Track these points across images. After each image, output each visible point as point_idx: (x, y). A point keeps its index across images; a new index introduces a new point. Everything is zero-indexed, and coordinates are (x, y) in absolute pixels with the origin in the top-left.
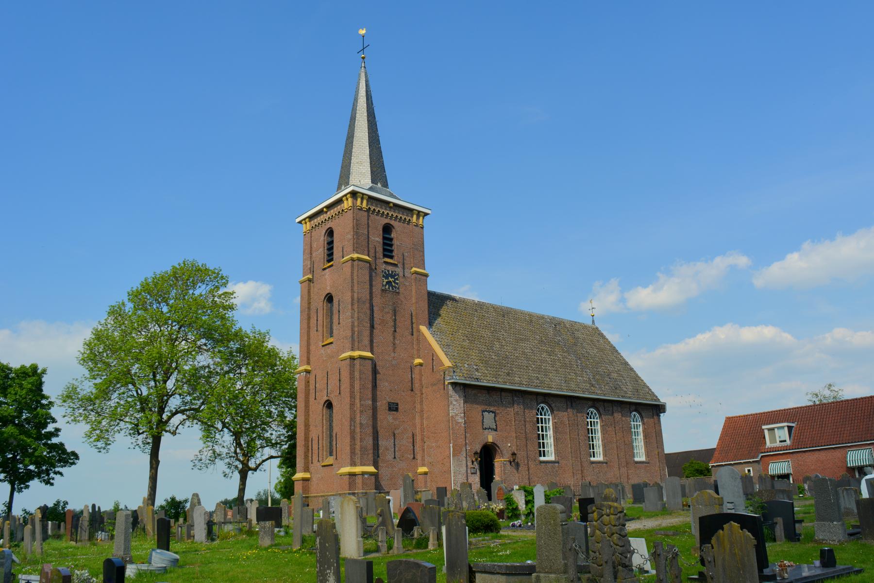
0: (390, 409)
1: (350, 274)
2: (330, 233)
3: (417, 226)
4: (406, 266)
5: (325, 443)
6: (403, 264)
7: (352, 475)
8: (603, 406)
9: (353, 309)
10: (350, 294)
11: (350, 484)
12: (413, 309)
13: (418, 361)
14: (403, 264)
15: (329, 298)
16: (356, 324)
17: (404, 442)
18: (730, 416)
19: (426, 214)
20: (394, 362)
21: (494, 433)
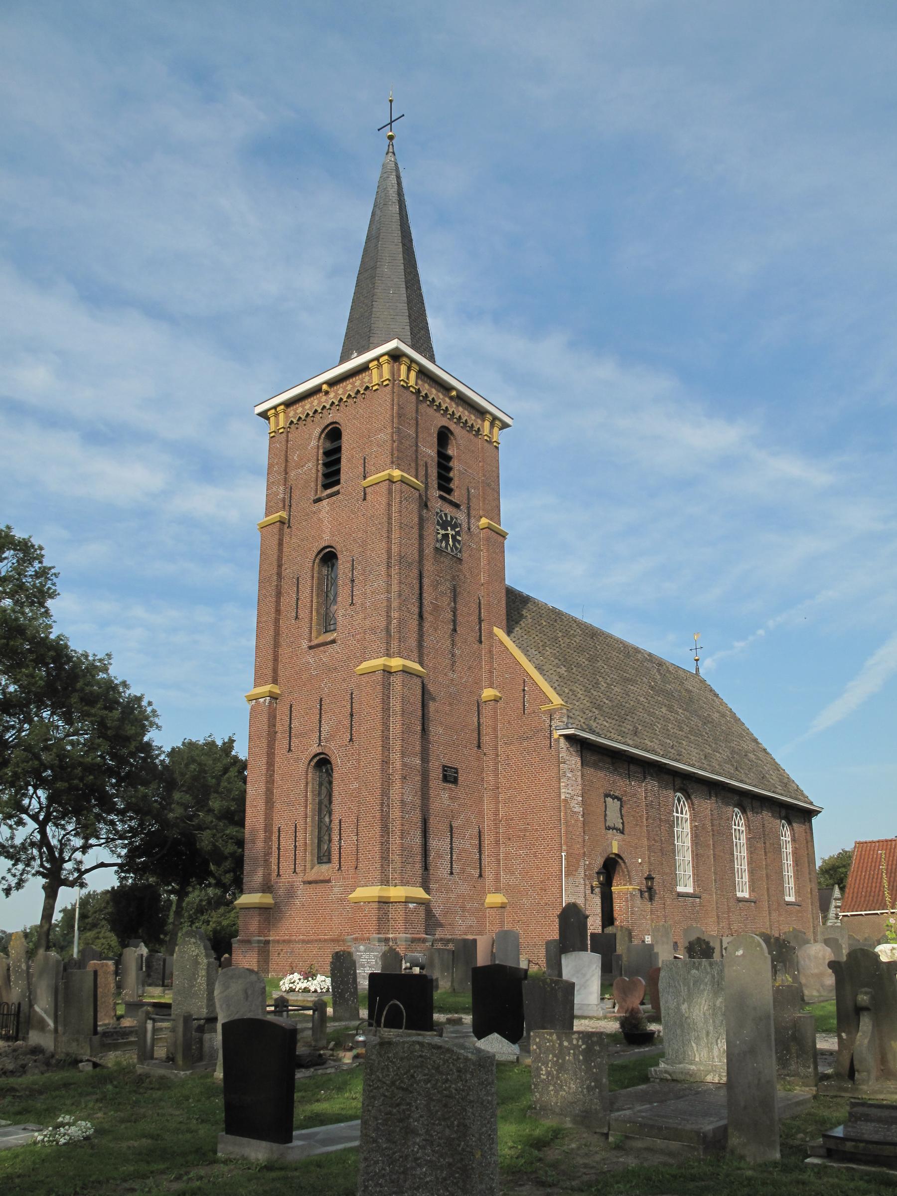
0: (446, 779)
1: (276, 557)
2: (334, 434)
3: (490, 442)
4: (473, 513)
5: (307, 837)
6: (469, 508)
7: (384, 902)
8: (747, 801)
9: (389, 576)
10: (384, 545)
11: (379, 919)
12: (482, 593)
13: (488, 693)
14: (469, 508)
15: (328, 557)
16: (395, 604)
17: (466, 843)
18: (863, 840)
19: (505, 425)
20: (452, 689)
21: (619, 836)
